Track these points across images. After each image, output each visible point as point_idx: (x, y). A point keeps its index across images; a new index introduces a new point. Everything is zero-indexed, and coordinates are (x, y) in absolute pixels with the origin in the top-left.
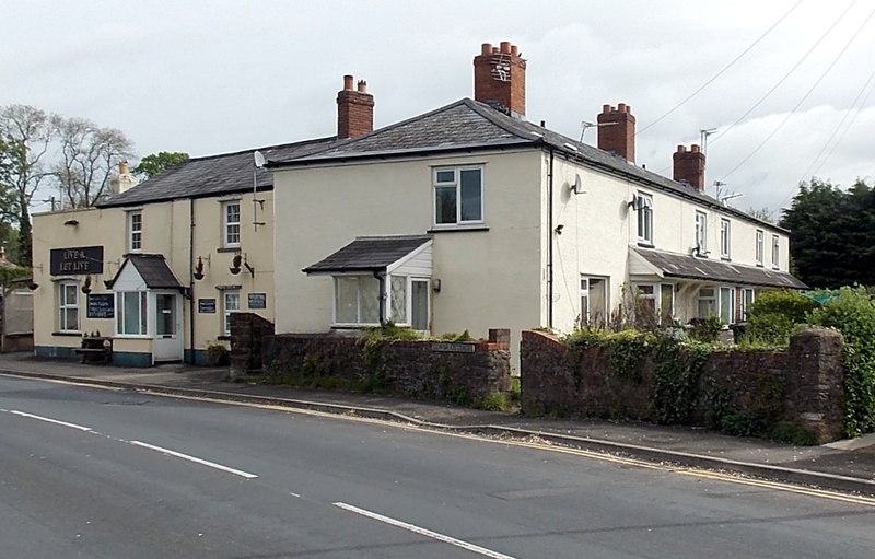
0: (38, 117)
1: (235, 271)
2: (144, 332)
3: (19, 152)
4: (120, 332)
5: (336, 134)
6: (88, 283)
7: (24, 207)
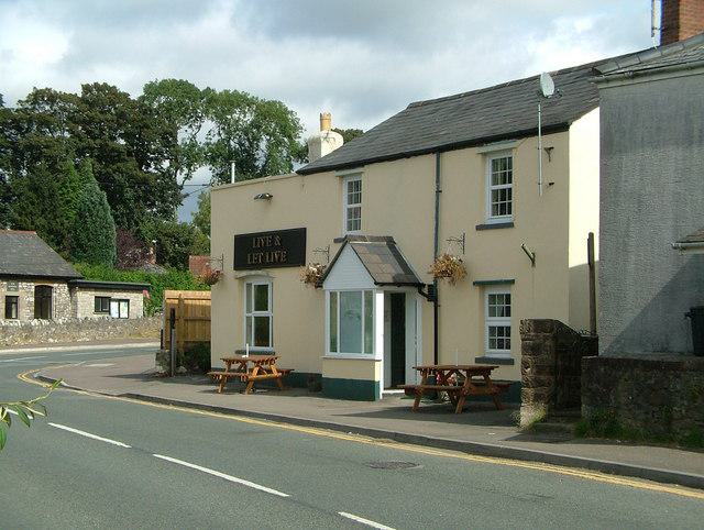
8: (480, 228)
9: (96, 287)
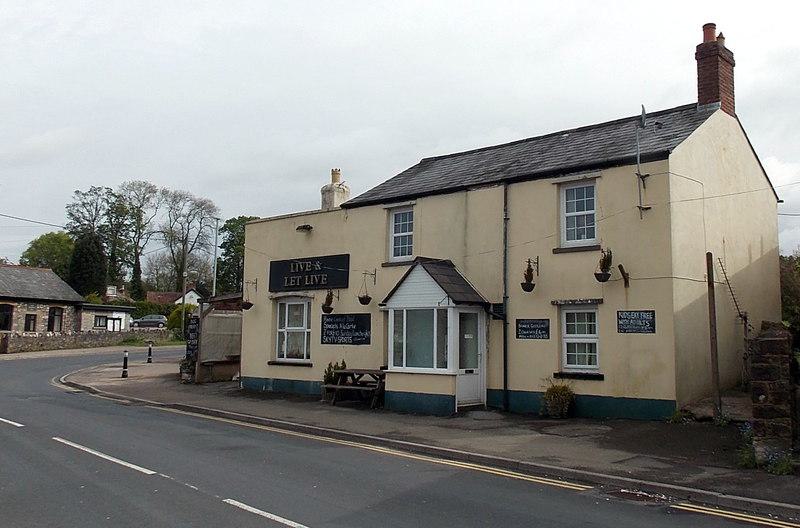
0: (152, 190)
1: (602, 277)
2: (444, 365)
3: (137, 214)
4: (398, 362)
5: (696, 101)
6: (329, 300)
7: (137, 255)
8: (556, 251)
9: (96, 309)
